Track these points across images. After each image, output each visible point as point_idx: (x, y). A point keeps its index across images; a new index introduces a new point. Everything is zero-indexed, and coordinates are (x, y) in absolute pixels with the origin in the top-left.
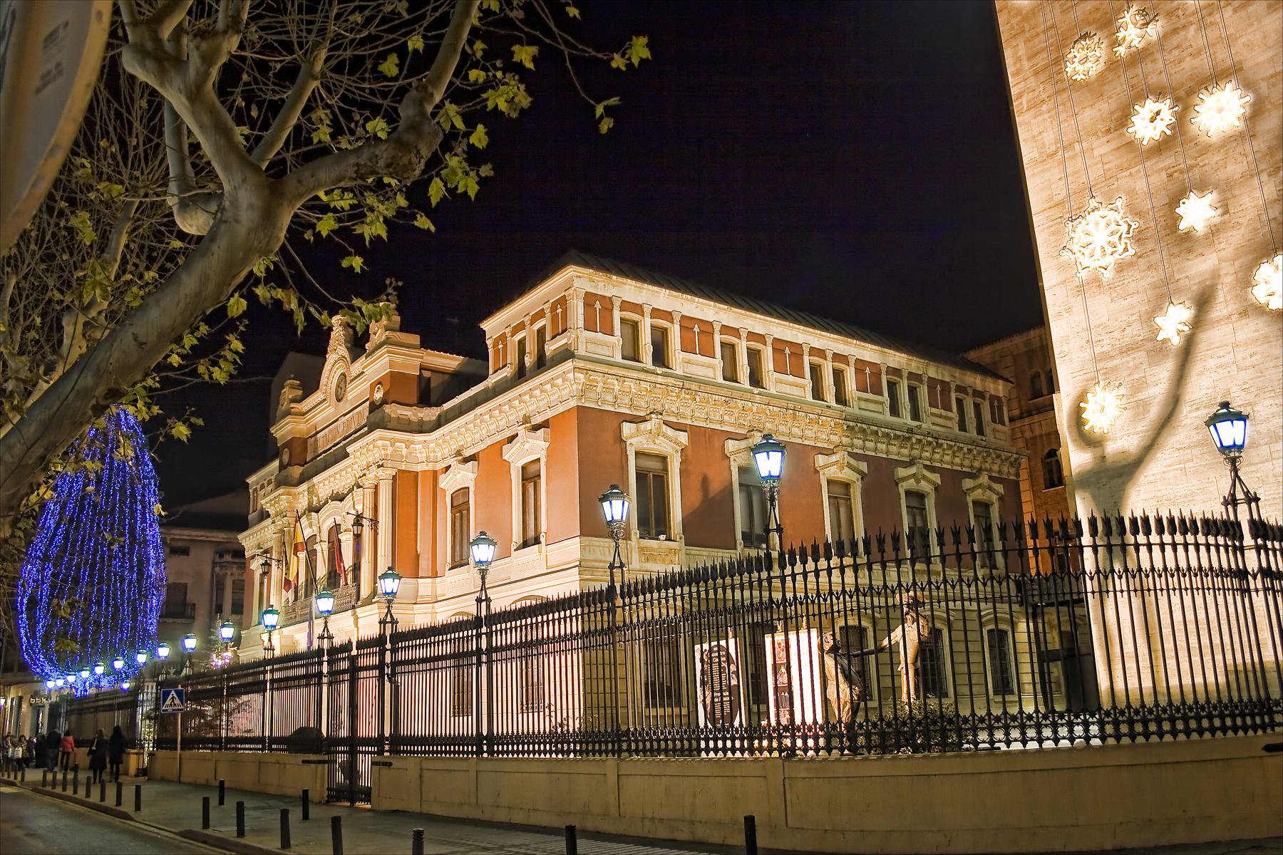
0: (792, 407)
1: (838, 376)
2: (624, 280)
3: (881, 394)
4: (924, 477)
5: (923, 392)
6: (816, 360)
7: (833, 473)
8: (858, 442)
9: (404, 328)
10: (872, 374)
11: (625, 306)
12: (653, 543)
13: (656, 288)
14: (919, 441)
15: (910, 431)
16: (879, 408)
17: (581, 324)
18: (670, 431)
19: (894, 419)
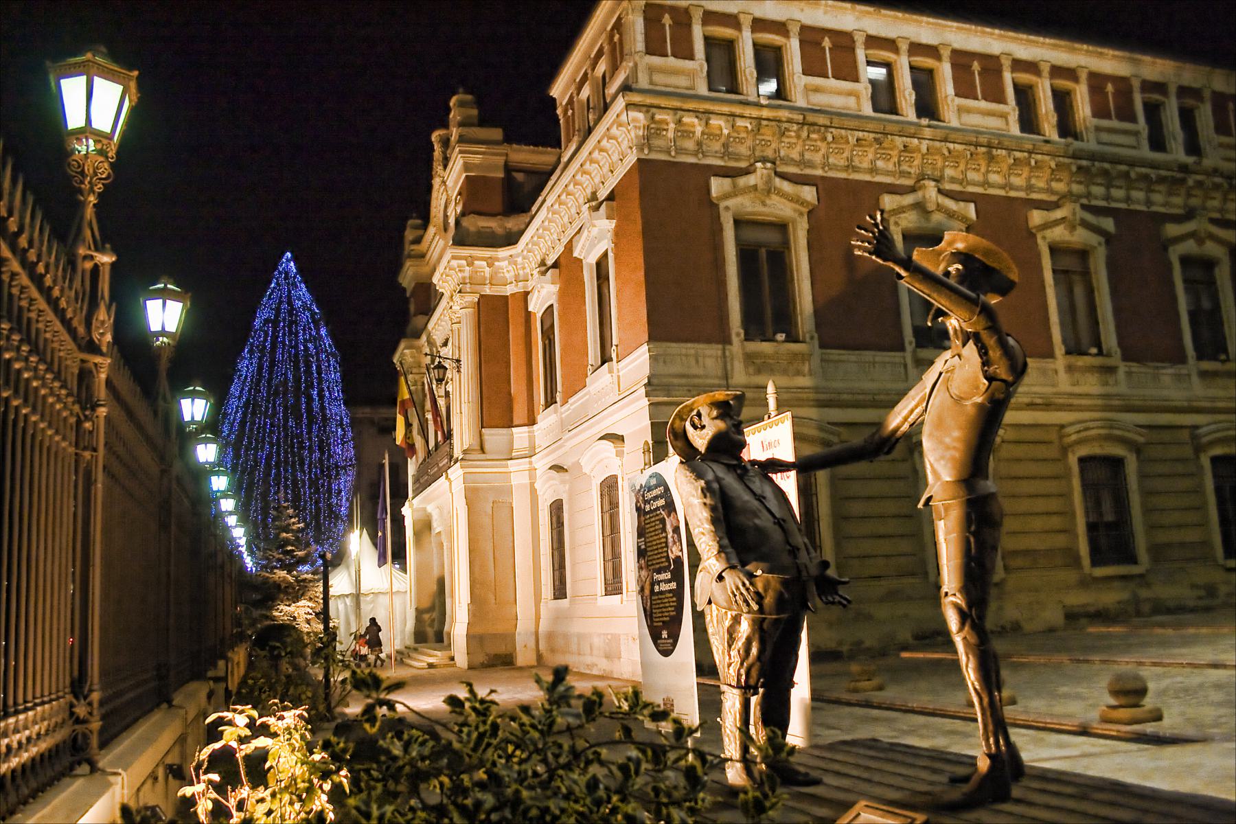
0: (988, 146)
1: (1062, 100)
3: (1132, 118)
4: (1212, 237)
5: (1205, 116)
6: (1024, 78)
7: (1059, 234)
8: (1098, 190)
9: (483, 122)
10: (1117, 93)
12: (766, 347)
14: (1200, 184)
15: (1184, 168)
16: (1130, 140)
17: (640, 45)
18: (786, 186)
19: (1158, 156)
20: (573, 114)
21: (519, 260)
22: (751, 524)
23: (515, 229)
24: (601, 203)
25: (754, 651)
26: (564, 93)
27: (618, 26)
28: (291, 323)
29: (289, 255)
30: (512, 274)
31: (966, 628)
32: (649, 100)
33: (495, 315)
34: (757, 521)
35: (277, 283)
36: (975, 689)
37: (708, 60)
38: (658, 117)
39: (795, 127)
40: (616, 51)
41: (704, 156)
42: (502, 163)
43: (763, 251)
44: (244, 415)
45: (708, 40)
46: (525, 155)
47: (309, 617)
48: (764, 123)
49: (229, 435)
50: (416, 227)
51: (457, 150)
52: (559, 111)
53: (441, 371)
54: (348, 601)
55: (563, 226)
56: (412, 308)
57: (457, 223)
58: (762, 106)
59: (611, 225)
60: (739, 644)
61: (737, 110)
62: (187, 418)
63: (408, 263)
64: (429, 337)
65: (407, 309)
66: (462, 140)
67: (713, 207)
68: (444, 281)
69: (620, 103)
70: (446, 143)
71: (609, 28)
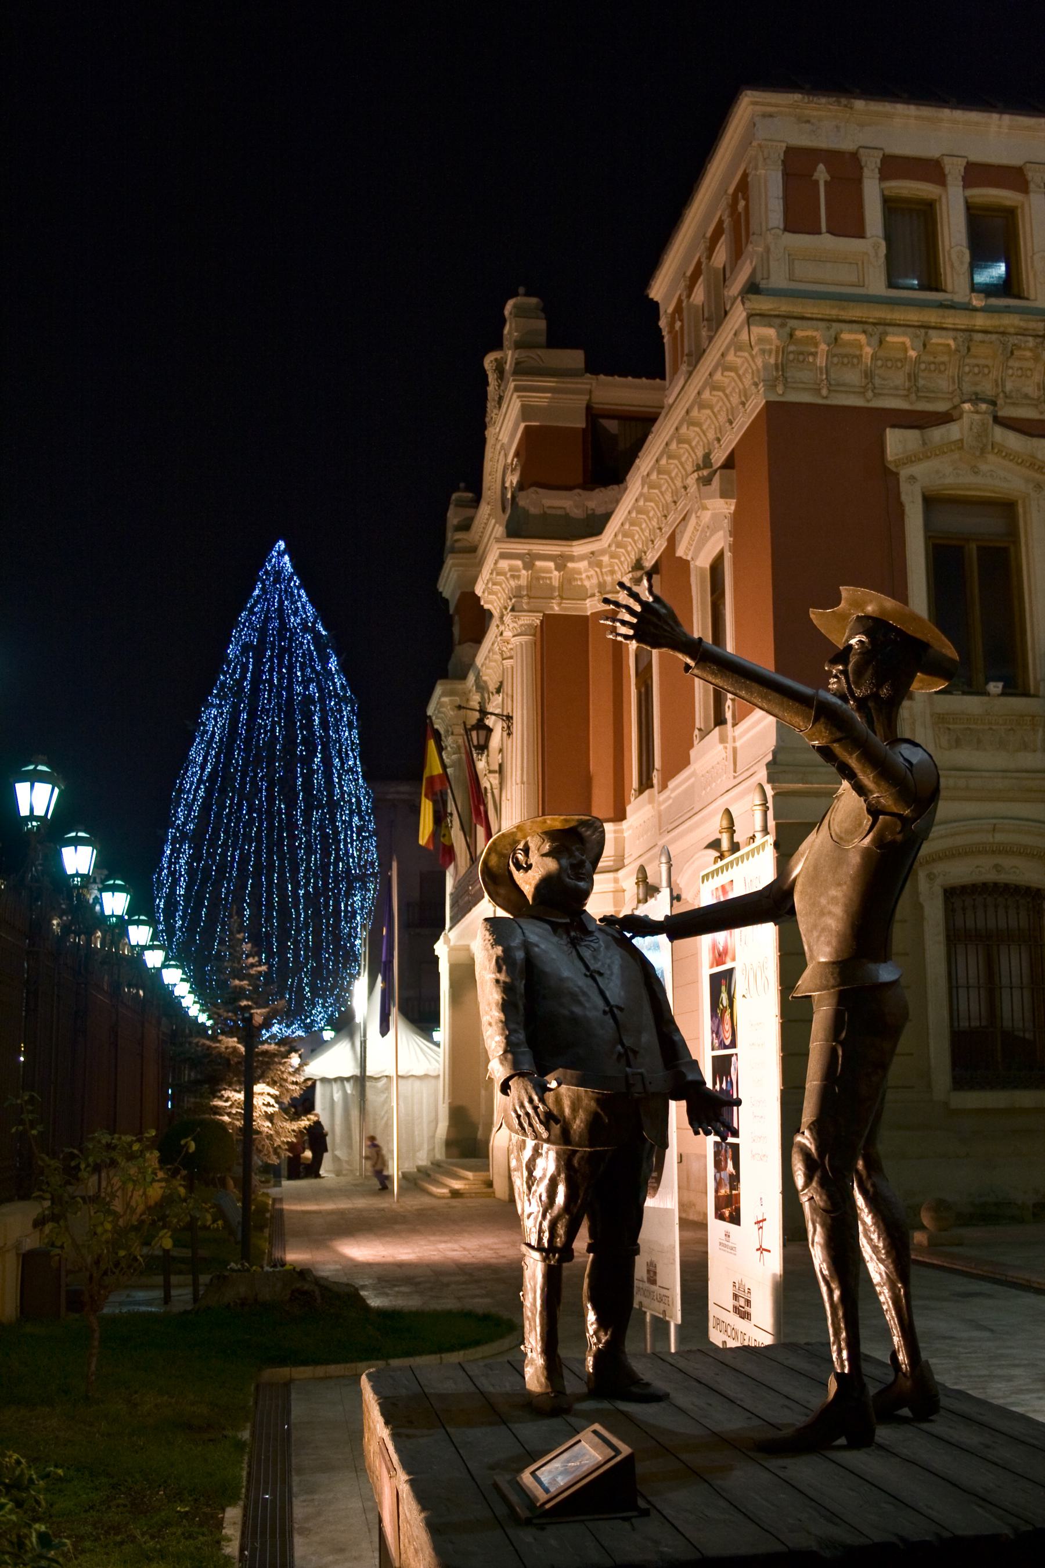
2: (886, 107)
9: (555, 340)
11: (894, 166)
13: (974, 116)
17: (775, 215)
18: (1013, 440)
20: (682, 327)
21: (605, 559)
22: (566, 1012)
23: (600, 511)
24: (715, 471)
25: (560, 1199)
26: (668, 297)
27: (743, 186)
28: (283, 650)
29: (281, 545)
30: (595, 581)
31: (814, 1184)
32: (785, 307)
33: (562, 645)
34: (577, 1010)
35: (263, 590)
36: (823, 1276)
37: (888, 238)
38: (799, 334)
39: (1031, 342)
40: (737, 227)
41: (876, 395)
42: (583, 405)
43: (973, 546)
44: (209, 792)
45: (891, 206)
46: (621, 392)
47: (270, 1110)
48: (978, 337)
49: (185, 824)
50: (461, 504)
51: (512, 385)
52: (663, 323)
53: (483, 733)
54: (349, 1087)
55: (666, 507)
56: (456, 630)
57: (513, 497)
58: (975, 309)
59: (726, 507)
60: (541, 1189)
61: (932, 317)
62: (24, 812)
63: (450, 561)
64: (478, 677)
65: (450, 632)
66: (519, 370)
67: (887, 479)
68: (492, 588)
69: (738, 314)
70: (500, 370)
71: (731, 191)
